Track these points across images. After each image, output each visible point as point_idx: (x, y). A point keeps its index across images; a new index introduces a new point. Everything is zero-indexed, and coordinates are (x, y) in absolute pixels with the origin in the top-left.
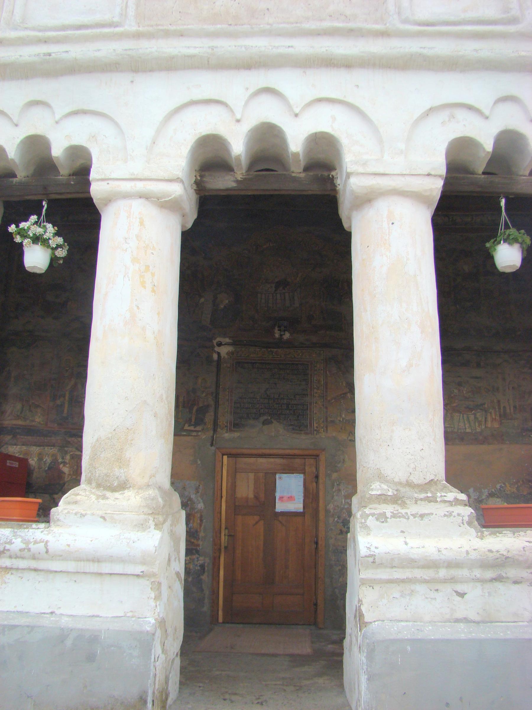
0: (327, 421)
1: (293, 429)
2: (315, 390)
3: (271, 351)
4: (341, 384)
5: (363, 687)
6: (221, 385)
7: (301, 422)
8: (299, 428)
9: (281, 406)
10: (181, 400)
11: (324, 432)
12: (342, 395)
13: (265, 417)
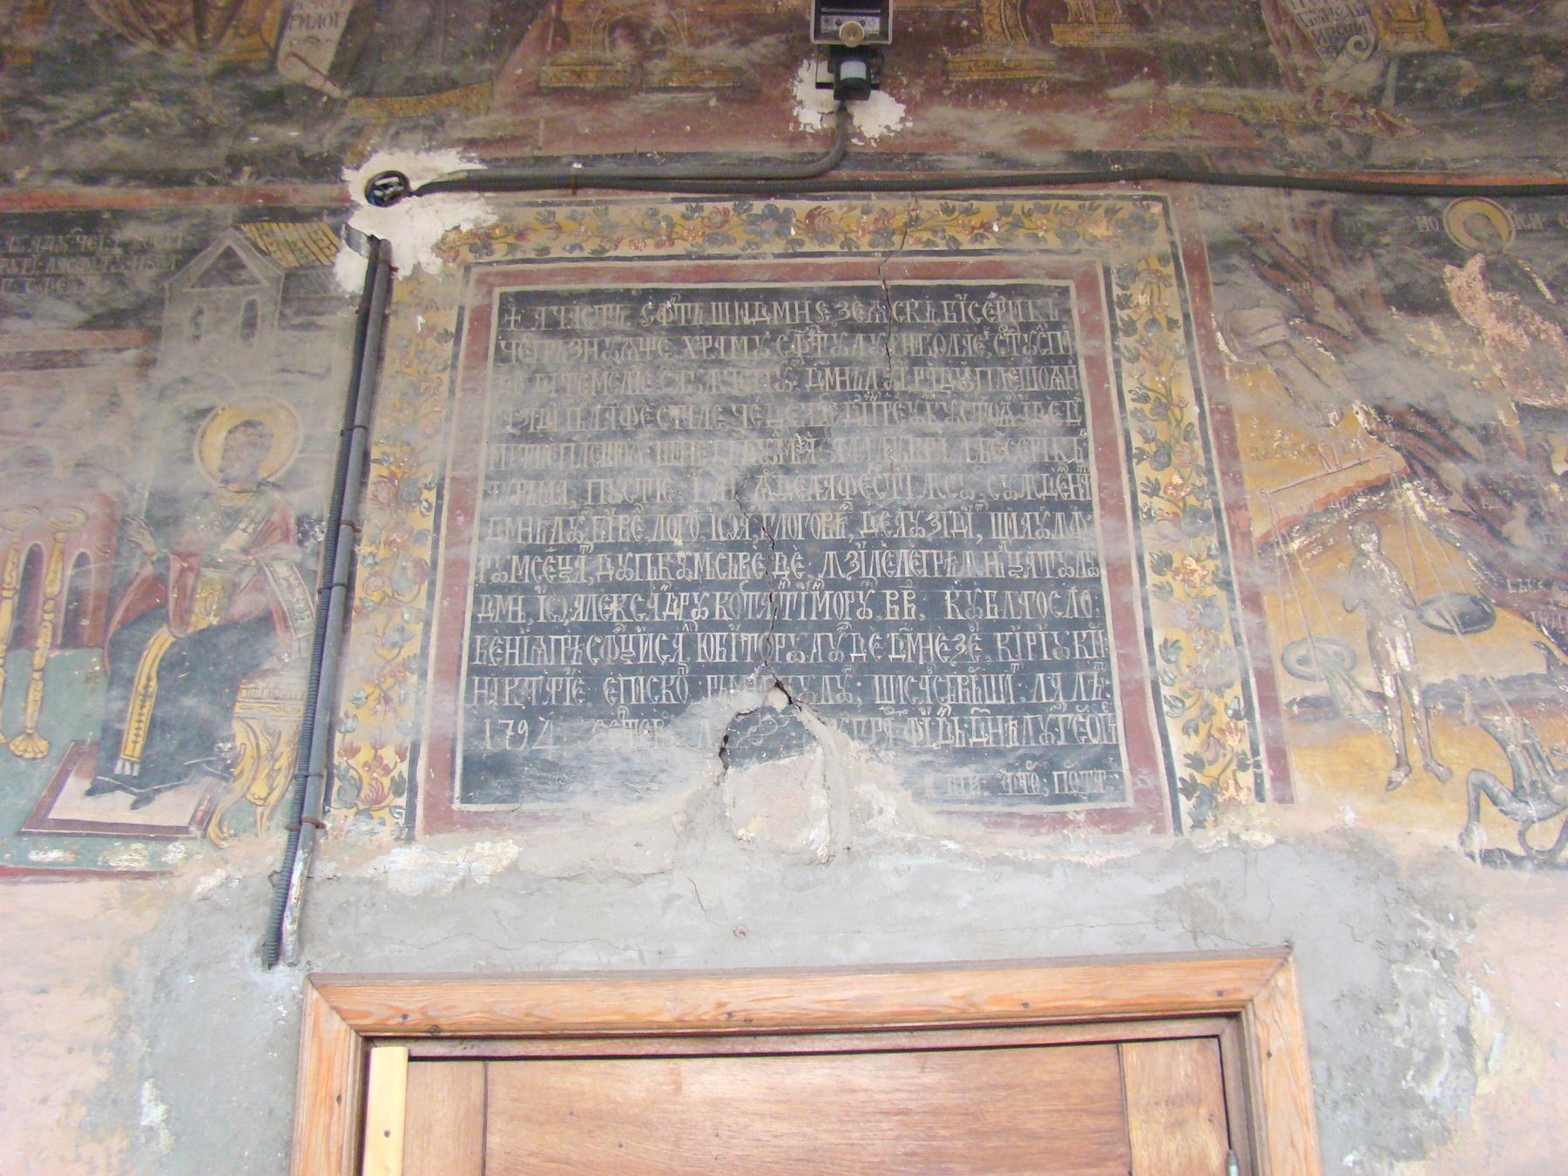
0: (1270, 703)
1: (994, 788)
2: (1143, 471)
3: (772, 213)
4: (1333, 416)
5: (753, 149)
6: (377, 461)
7: (1053, 726)
8: (1045, 774)
9: (877, 603)
10: (55, 589)
11: (1260, 795)
12: (1362, 500)
13: (746, 698)
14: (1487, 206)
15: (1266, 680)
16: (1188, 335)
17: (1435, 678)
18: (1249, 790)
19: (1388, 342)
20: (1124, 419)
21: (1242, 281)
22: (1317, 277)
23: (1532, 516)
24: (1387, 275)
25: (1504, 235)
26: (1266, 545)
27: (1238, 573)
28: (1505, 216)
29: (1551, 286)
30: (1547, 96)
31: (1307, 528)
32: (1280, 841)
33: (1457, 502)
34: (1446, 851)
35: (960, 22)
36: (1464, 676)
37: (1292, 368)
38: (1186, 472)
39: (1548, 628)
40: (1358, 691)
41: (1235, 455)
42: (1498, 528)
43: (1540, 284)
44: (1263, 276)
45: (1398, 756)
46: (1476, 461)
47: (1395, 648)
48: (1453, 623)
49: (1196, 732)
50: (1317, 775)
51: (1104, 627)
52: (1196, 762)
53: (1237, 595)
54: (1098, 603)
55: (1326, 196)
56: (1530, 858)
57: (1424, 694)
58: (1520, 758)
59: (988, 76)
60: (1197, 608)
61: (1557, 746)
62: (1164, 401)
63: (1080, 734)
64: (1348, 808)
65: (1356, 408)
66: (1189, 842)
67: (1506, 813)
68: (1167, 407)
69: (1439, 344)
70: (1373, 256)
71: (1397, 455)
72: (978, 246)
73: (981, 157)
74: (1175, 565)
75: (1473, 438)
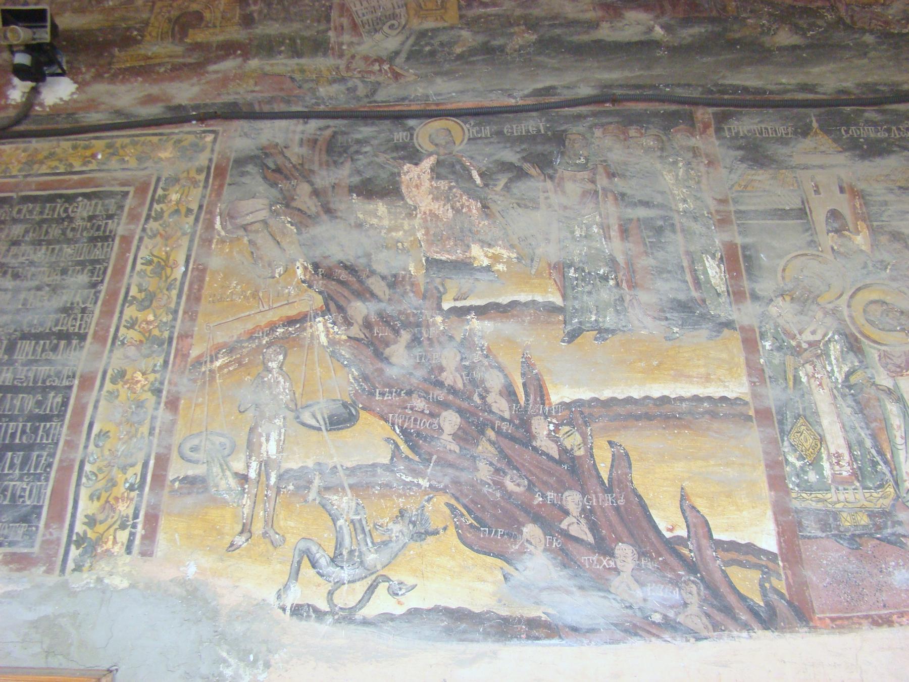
11: (129, 549)
14: (451, 123)
15: (162, 462)
16: (197, 220)
17: (294, 465)
18: (123, 544)
19: (341, 218)
20: (131, 276)
21: (248, 181)
22: (304, 177)
23: (413, 341)
24: (359, 172)
25: (457, 143)
26: (199, 362)
27: (170, 383)
28: (463, 129)
29: (481, 175)
30: (520, 51)
31: (231, 350)
32: (132, 586)
33: (355, 331)
34: (262, 605)
35: (132, 33)
36: (319, 464)
37: (262, 239)
38: (159, 312)
39: (401, 428)
40: (228, 473)
41: (198, 299)
42: (381, 350)
43: (475, 175)
44: (265, 178)
45: (244, 524)
46: (380, 301)
47: (268, 440)
48: (322, 422)
49: (99, 499)
50: (176, 536)
51: (63, 421)
52: (91, 521)
53: (164, 399)
54: (65, 404)
55: (331, 122)
56: (332, 613)
57: (280, 477)
58: (346, 531)
59: (136, 64)
60: (130, 408)
61: (381, 521)
62: (163, 263)
63: (21, 497)
64: (192, 563)
65: (298, 264)
66: (67, 582)
67: (322, 575)
68: (163, 268)
69: (380, 218)
70: (352, 160)
71: (320, 297)
72: (84, 168)
73: (111, 113)
74: (127, 377)
75: (383, 284)
